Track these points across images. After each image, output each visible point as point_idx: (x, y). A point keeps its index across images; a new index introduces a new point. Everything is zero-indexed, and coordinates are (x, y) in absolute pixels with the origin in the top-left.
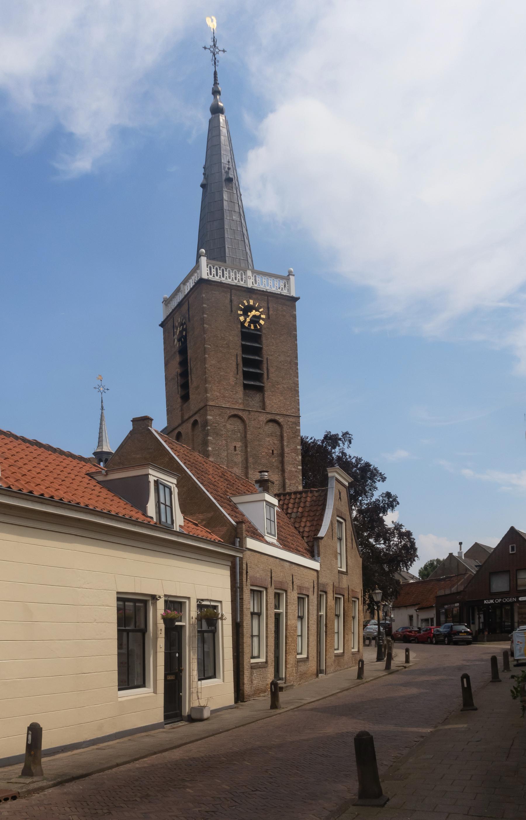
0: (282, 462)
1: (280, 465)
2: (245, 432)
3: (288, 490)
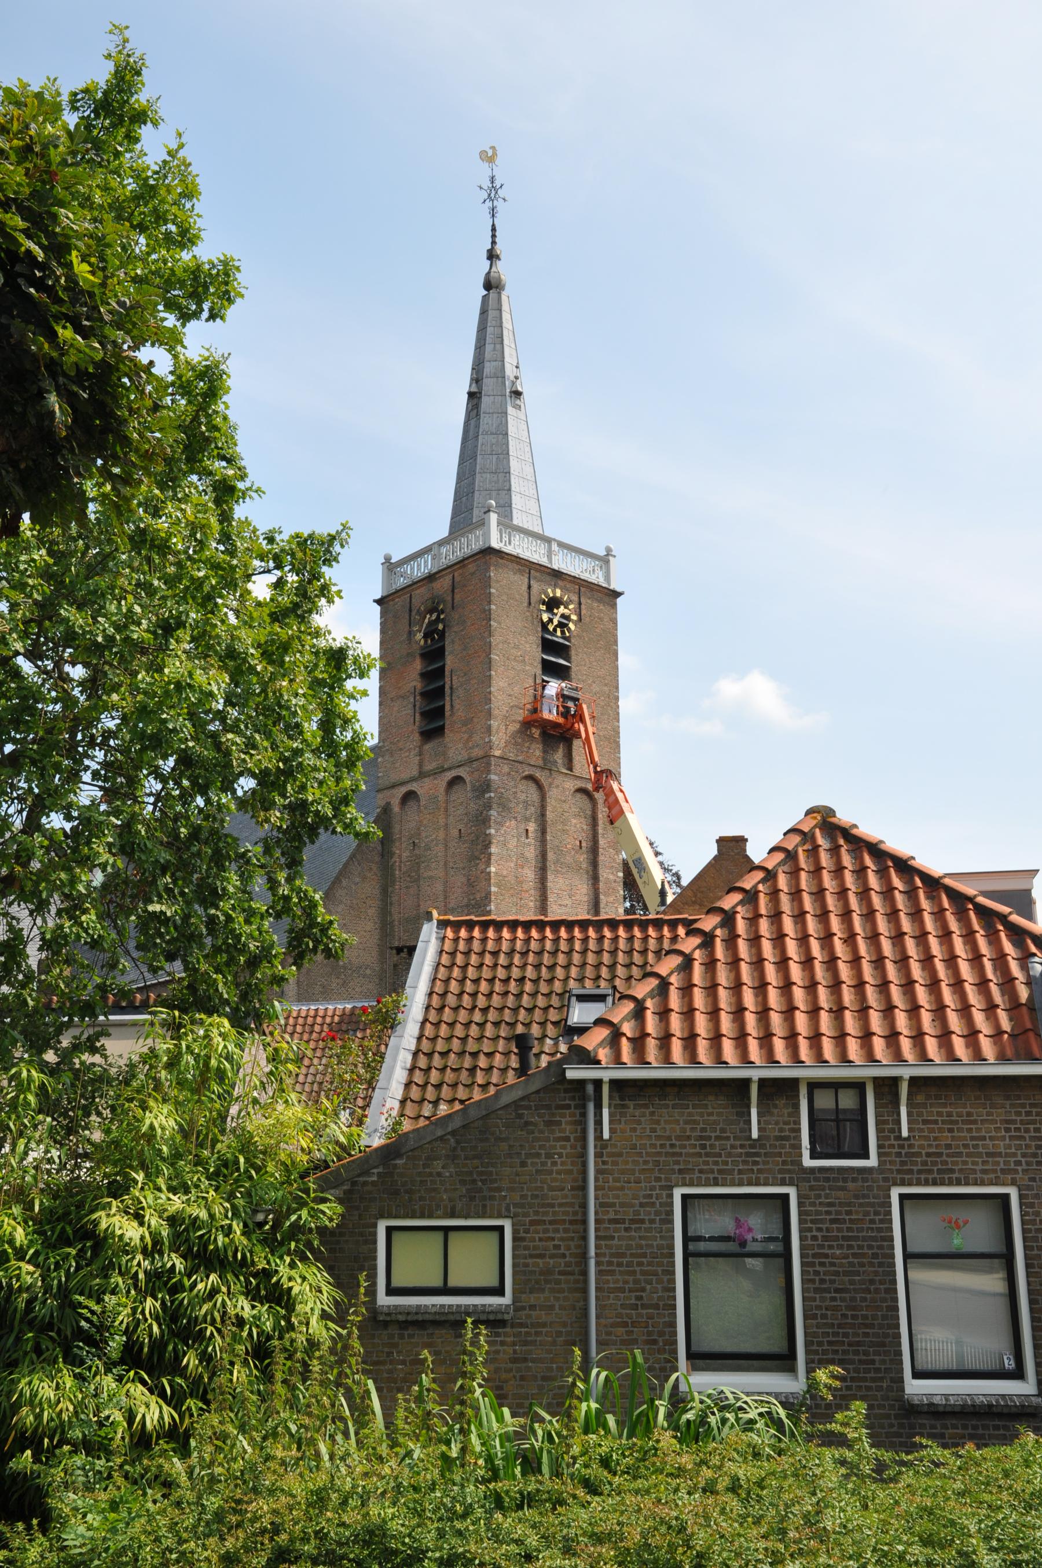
0: (594, 864)
1: (590, 868)
2: (543, 807)
3: (555, 913)
